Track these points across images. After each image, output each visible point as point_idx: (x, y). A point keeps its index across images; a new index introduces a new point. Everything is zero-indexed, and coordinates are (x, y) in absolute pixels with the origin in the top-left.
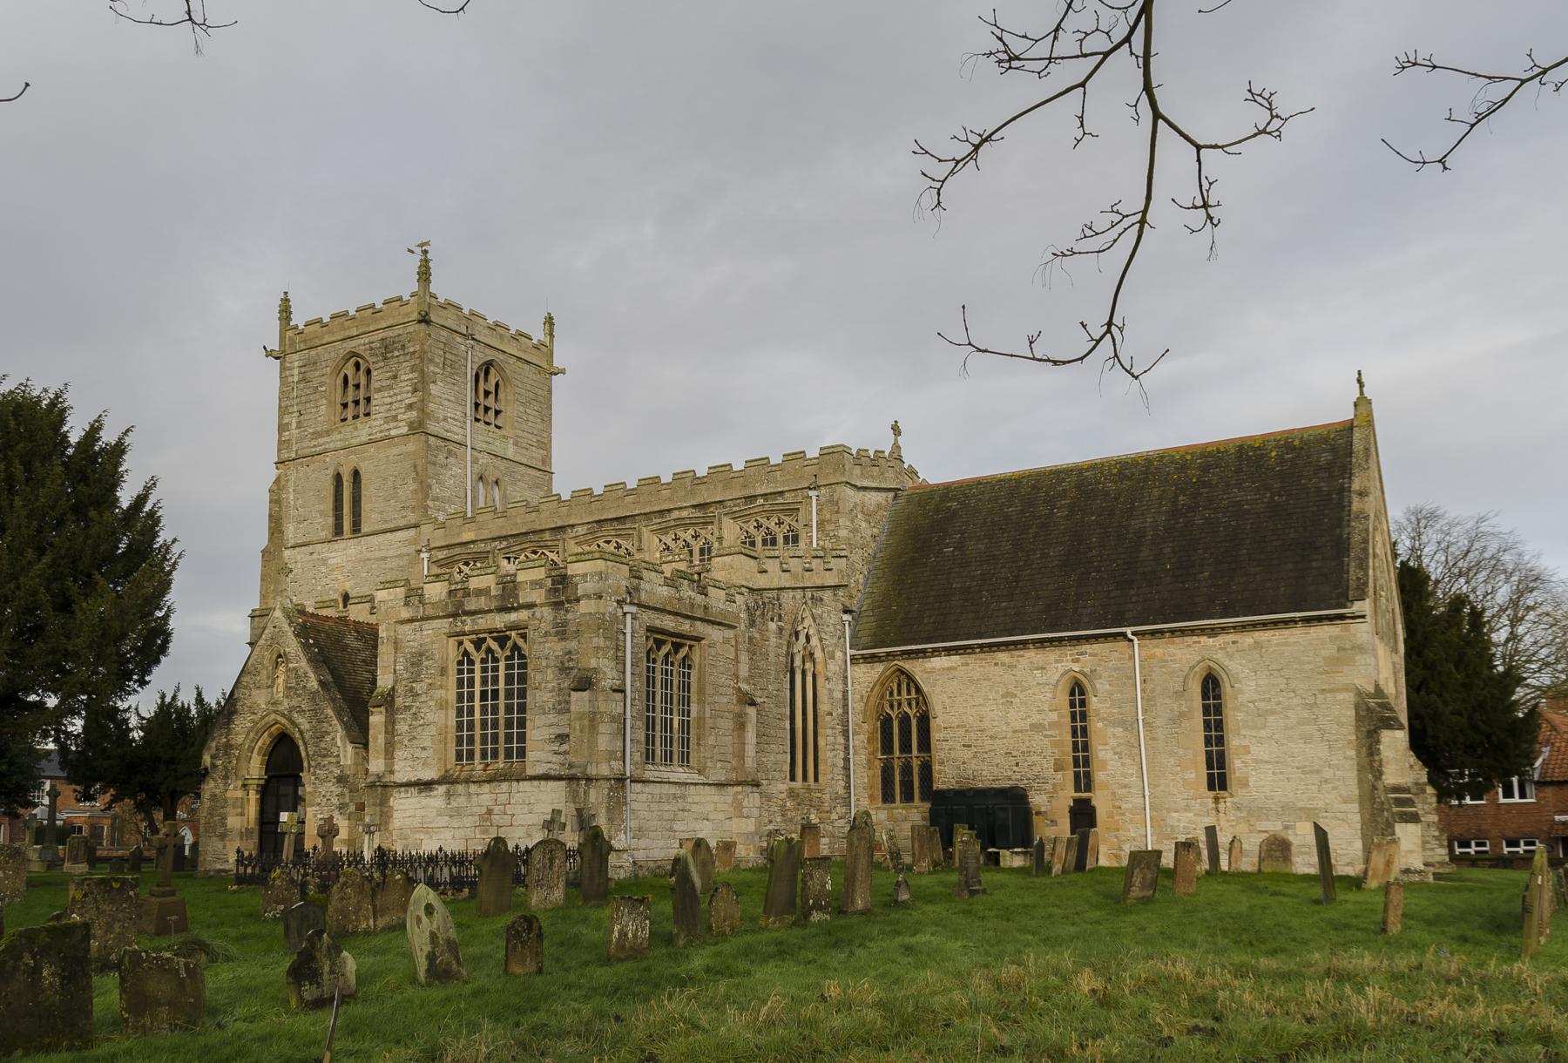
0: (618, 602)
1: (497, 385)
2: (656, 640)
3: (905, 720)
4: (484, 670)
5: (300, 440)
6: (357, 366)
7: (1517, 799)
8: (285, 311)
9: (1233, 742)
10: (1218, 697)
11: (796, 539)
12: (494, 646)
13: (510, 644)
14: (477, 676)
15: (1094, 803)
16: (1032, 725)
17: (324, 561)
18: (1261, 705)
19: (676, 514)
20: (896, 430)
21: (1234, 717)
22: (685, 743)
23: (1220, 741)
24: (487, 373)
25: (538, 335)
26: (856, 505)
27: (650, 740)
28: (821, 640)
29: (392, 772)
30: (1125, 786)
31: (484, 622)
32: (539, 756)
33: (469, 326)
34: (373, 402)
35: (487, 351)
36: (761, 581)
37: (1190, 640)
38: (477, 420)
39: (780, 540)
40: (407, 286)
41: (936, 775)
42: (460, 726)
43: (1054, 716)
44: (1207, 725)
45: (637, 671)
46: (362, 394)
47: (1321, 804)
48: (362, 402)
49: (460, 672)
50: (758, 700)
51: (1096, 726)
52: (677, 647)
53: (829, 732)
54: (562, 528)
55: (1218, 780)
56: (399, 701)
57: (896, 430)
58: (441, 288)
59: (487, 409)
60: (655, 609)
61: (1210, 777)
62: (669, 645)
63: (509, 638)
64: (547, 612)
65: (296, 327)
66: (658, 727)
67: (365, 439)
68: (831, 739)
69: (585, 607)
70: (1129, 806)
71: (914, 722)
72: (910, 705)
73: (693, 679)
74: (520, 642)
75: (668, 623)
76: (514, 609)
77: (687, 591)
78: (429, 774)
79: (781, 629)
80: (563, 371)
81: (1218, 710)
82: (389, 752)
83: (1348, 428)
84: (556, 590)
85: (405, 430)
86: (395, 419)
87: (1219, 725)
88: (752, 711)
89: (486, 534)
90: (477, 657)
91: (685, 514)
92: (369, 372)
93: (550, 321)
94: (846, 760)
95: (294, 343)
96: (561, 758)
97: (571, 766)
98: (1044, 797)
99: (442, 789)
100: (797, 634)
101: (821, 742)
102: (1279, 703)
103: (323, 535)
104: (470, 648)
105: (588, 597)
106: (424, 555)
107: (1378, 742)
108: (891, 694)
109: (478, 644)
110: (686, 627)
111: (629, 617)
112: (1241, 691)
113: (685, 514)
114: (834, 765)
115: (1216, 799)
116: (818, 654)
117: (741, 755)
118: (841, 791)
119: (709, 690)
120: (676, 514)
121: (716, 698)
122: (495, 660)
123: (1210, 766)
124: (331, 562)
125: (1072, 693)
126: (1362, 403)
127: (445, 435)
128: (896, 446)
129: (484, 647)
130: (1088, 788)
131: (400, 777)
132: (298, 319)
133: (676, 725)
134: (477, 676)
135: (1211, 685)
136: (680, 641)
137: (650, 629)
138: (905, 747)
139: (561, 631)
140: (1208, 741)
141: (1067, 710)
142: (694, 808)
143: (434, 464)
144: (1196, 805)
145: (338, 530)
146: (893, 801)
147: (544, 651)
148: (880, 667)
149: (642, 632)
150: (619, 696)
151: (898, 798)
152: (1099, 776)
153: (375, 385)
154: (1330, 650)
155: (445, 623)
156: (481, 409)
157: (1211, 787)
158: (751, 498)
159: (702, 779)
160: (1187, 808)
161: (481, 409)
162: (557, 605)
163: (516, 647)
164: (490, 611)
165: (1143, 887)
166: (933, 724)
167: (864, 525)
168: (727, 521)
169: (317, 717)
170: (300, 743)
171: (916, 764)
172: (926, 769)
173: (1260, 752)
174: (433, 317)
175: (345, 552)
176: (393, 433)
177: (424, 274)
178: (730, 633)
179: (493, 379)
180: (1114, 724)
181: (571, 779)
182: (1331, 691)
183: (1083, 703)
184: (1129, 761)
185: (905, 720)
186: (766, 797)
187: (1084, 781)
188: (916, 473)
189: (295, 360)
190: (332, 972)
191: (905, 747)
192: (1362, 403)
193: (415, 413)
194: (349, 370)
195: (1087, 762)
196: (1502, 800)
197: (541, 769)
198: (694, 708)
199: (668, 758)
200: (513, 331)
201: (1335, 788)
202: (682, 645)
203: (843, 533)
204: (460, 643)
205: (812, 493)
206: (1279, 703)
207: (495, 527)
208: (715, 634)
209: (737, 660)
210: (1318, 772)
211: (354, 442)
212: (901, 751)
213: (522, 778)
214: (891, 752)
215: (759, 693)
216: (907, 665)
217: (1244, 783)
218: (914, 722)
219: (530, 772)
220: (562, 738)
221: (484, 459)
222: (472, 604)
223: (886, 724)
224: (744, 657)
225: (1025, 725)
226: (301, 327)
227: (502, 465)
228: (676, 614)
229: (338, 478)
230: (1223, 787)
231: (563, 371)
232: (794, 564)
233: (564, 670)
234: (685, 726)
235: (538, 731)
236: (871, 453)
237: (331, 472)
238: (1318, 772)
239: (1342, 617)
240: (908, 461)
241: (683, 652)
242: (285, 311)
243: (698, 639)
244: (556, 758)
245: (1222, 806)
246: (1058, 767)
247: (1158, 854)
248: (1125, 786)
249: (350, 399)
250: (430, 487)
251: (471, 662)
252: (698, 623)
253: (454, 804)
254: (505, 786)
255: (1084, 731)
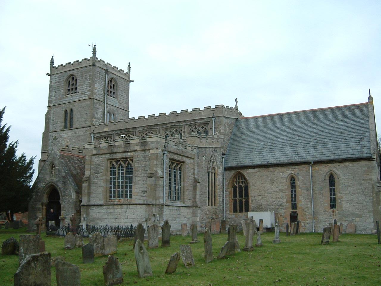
0: (162, 150)
1: (114, 85)
2: (172, 162)
3: (241, 187)
4: (119, 170)
5: (55, 100)
6: (73, 78)
8: (52, 62)
9: (338, 195)
10: (334, 181)
11: (207, 132)
13: (127, 162)
14: (117, 172)
15: (297, 212)
16: (279, 189)
17: (61, 136)
18: (346, 184)
22: (180, 194)
23: (334, 194)
24: (111, 81)
25: (126, 70)
26: (226, 123)
27: (170, 193)
28: (217, 163)
32: (137, 198)
33: (107, 69)
34: (78, 89)
35: (112, 75)
36: (201, 146)
38: (108, 95)
39: (202, 132)
40: (89, 55)
41: (250, 204)
43: (286, 187)
44: (331, 190)
45: (167, 171)
46: (74, 87)
50: (200, 181)
51: (298, 190)
52: (177, 164)
53: (218, 191)
54: (135, 128)
55: (333, 206)
59: (111, 92)
60: (172, 153)
61: (331, 205)
62: (176, 164)
65: (55, 67)
66: (172, 189)
68: (219, 193)
69: (152, 151)
70: (308, 213)
72: (242, 183)
73: (182, 175)
74: (131, 162)
75: (176, 157)
77: (181, 147)
81: (334, 185)
82: (89, 194)
83: (366, 104)
87: (334, 190)
88: (198, 184)
91: (173, 124)
92: (76, 80)
93: (129, 67)
95: (55, 72)
98: (283, 211)
101: (216, 194)
102: (351, 184)
104: (114, 163)
106: (92, 135)
108: (236, 180)
111: (165, 155)
112: (341, 180)
113: (173, 124)
114: (220, 201)
115: (333, 211)
116: (216, 167)
118: (222, 209)
121: (188, 180)
122: (122, 167)
123: (331, 202)
125: (291, 180)
126: (370, 98)
128: (236, 106)
130: (296, 208)
132: (56, 65)
133: (177, 188)
134: (117, 172)
135: (332, 178)
136: (179, 162)
137: (170, 159)
138: (241, 196)
142: (182, 214)
143: (95, 108)
144: (327, 213)
145: (65, 127)
149: (168, 159)
151: (238, 211)
152: (299, 205)
153: (78, 84)
155: (108, 156)
156: (109, 92)
157: (331, 208)
160: (325, 214)
161: (109, 92)
163: (129, 163)
165: (327, 238)
166: (250, 189)
167: (228, 129)
168: (186, 127)
169: (65, 183)
173: (347, 198)
174: (96, 64)
175: (67, 134)
176: (83, 98)
177: (94, 52)
178: (192, 161)
179: (113, 83)
180: (303, 189)
181: (147, 205)
182: (366, 180)
183: (294, 183)
184: (308, 200)
185: (241, 187)
186: (202, 211)
187: (294, 206)
188: (241, 114)
191: (241, 196)
192: (370, 98)
193: (90, 93)
194: (71, 80)
195: (295, 201)
198: (182, 183)
199: (175, 199)
200: (119, 69)
202: (178, 164)
206: (351, 184)
208: (188, 161)
209: (194, 169)
215: (200, 179)
216: (242, 171)
217: (341, 207)
219: (133, 202)
222: (115, 150)
223: (235, 188)
224: (196, 168)
225: (277, 189)
227: (115, 109)
230: (335, 207)
232: (209, 140)
234: (180, 188)
236: (225, 107)
237: (64, 110)
238: (362, 203)
240: (240, 110)
241: (179, 166)
242: (52, 62)
243: (184, 162)
244: (142, 198)
245: (335, 214)
250: (94, 115)
251: (115, 168)
255: (295, 191)
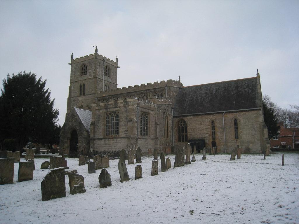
1: (108, 69)
3: (183, 127)
4: (111, 118)
6: (84, 66)
7: (275, 140)
8: (72, 57)
9: (240, 131)
12: (113, 114)
17: (78, 100)
19: (141, 92)
20: (179, 77)
21: (240, 126)
23: (237, 131)
24: (107, 68)
25: (115, 61)
27: (141, 131)
29: (95, 137)
30: (221, 138)
31: (111, 110)
32: (122, 134)
33: (104, 59)
34: (87, 72)
37: (233, 113)
41: (188, 137)
42: (107, 129)
43: (209, 127)
44: (235, 128)
47: (254, 141)
48: (85, 72)
49: (107, 119)
51: (216, 128)
52: (145, 115)
55: (237, 137)
56: (96, 124)
57: (179, 77)
58: (99, 53)
61: (236, 137)
63: (116, 113)
64: (123, 108)
67: (86, 78)
68: (170, 131)
70: (222, 142)
71: (181, 128)
75: (144, 110)
76: (117, 107)
78: (101, 137)
79: (162, 111)
80: (119, 67)
81: (237, 125)
83: (255, 78)
84: (125, 104)
85: (93, 77)
86: (91, 75)
87: (237, 128)
89: (107, 95)
90: (110, 116)
91: (143, 91)
92: (86, 67)
94: (173, 134)
96: (126, 134)
97: (128, 136)
99: (104, 140)
100: (165, 112)
101: (169, 131)
103: (78, 95)
105: (131, 105)
107: (264, 130)
108: (180, 123)
109: (110, 114)
110: (147, 111)
117: (156, 133)
119: (151, 122)
120: (141, 92)
122: (113, 117)
123: (236, 135)
124: (80, 100)
125: (212, 123)
126: (258, 74)
127: (100, 78)
128: (179, 80)
129: (111, 114)
131: (96, 137)
132: (74, 58)
135: (236, 121)
136: (146, 113)
139: (126, 112)
140: (235, 131)
141: (211, 126)
145: (81, 95)
146: (181, 142)
147: (123, 115)
148: (178, 118)
150: (136, 123)
151: (185, 141)
153: (87, 69)
154: (255, 115)
155: (104, 110)
157: (236, 139)
158: (155, 89)
159: (150, 138)
162: (125, 107)
163: (117, 114)
164: (113, 108)
166: (188, 128)
170: (77, 131)
171: (184, 135)
172: (186, 136)
173: (245, 132)
177: (96, 50)
178: (154, 112)
182: (255, 122)
185: (183, 127)
189: (74, 65)
190: (107, 177)
191: (183, 132)
192: (258, 74)
193: (94, 74)
196: (273, 140)
197: (122, 136)
199: (144, 134)
200: (111, 60)
201: (256, 138)
203: (171, 95)
204: (107, 114)
205: (166, 88)
207: (108, 94)
208: (152, 112)
209: (155, 117)
210: (254, 135)
211: (84, 79)
212: (185, 133)
213: (118, 138)
214: (180, 133)
216: (183, 118)
218: (181, 128)
220: (126, 131)
221: (106, 82)
223: (179, 128)
224: (156, 116)
226: (75, 59)
228: (146, 108)
229: (81, 85)
230: (238, 138)
231: (119, 67)
233: (127, 118)
235: (122, 129)
237: (80, 84)
239: (257, 110)
242: (72, 57)
246: (210, 135)
247: (78, 143)
248: (221, 138)
249: (83, 71)
252: (149, 110)
253: (106, 142)
254: (115, 139)
255: (214, 129)
